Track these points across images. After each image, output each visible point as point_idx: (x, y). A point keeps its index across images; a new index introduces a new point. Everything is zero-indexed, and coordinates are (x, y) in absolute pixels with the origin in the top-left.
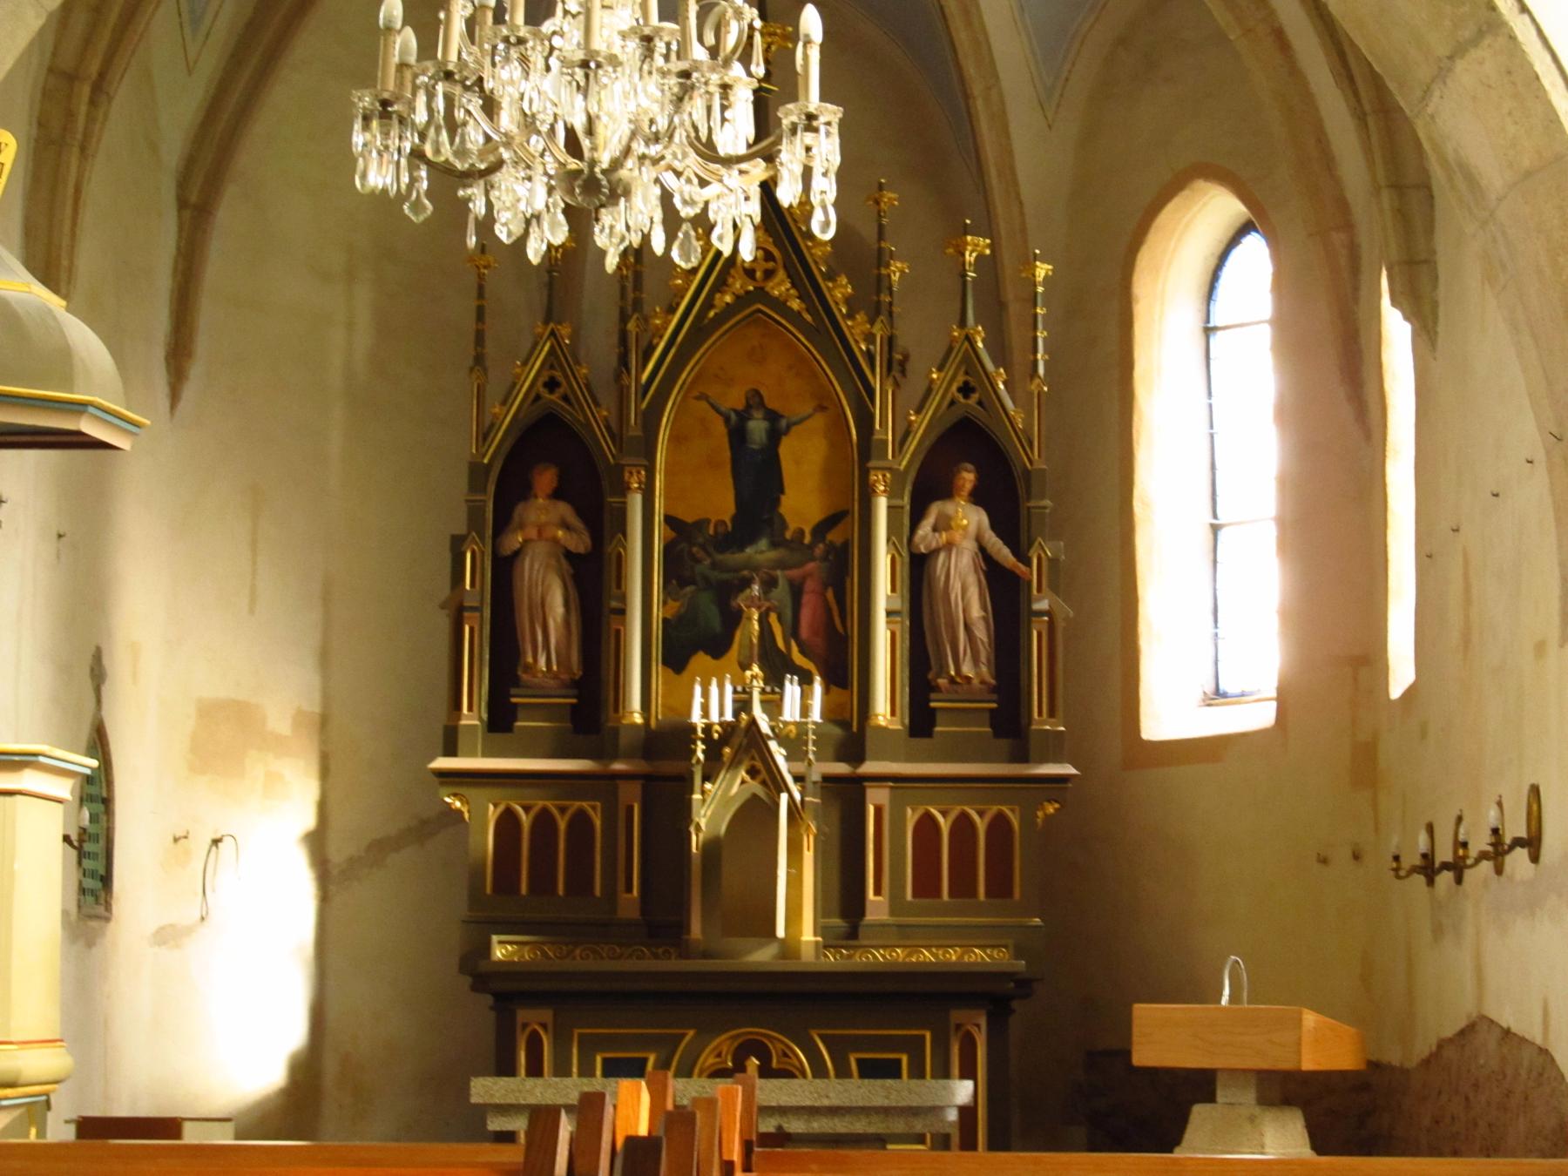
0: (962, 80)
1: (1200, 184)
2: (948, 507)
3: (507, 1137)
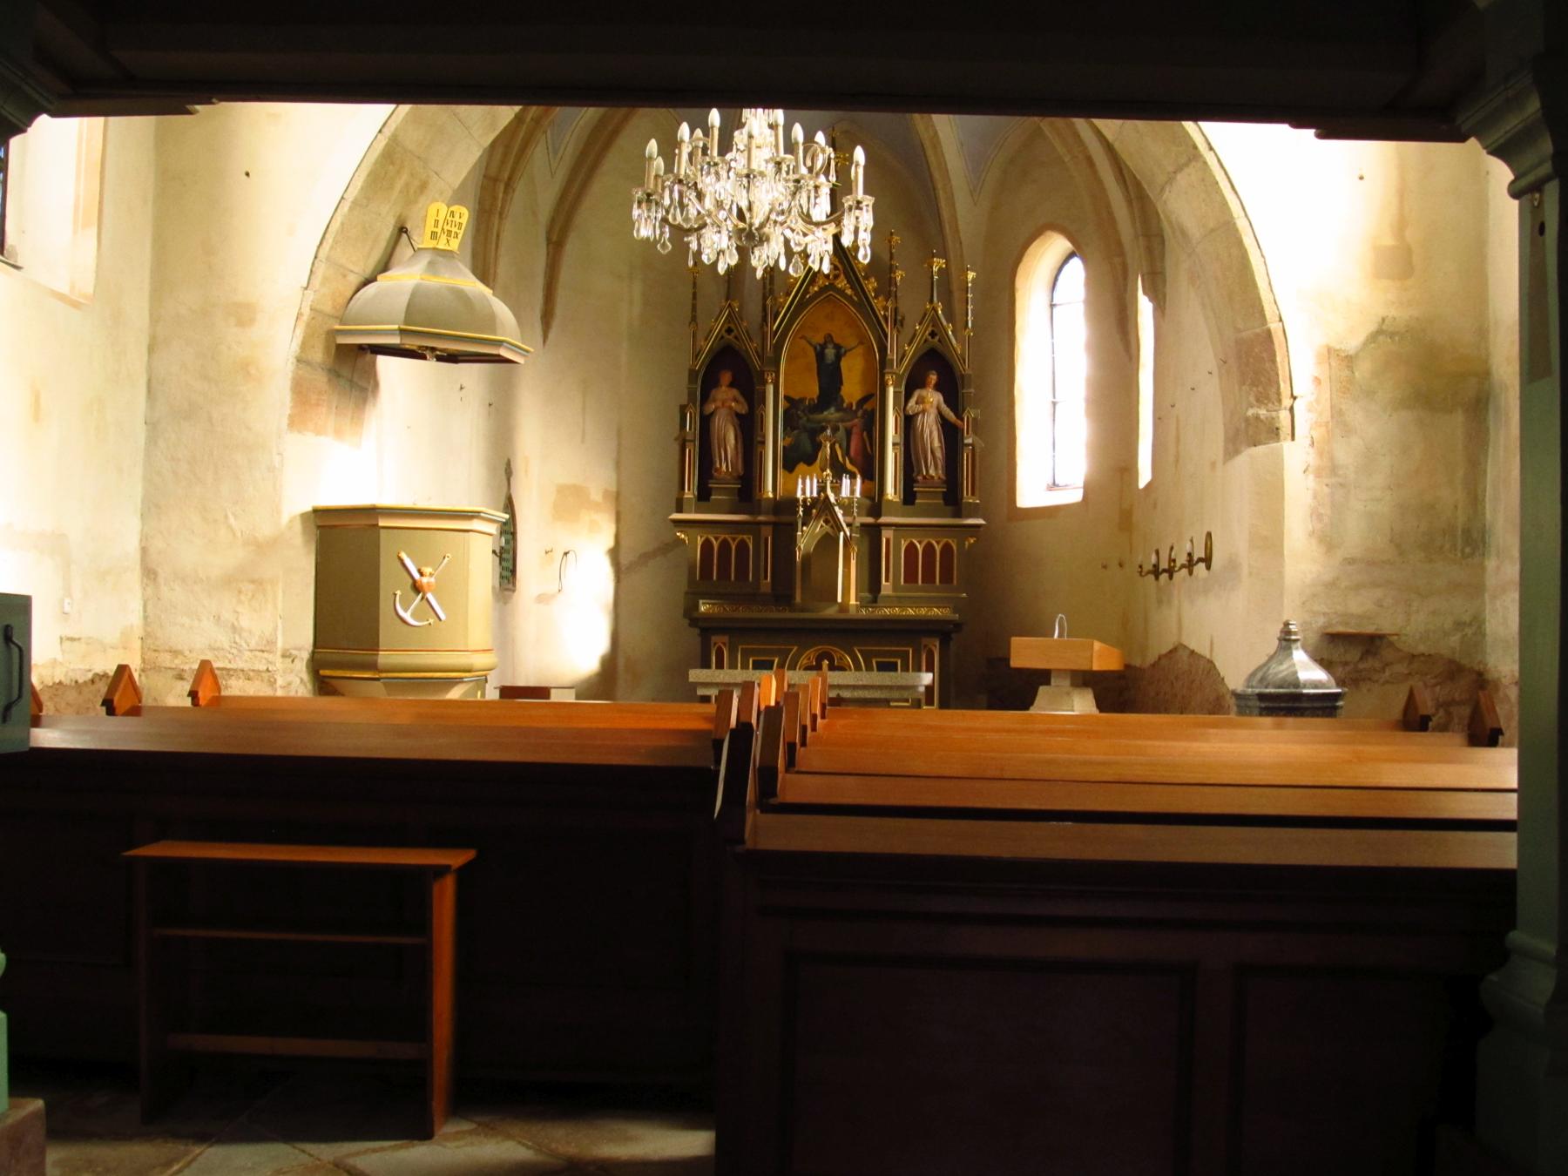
0: (931, 176)
1: (1049, 233)
2: (923, 392)
3: (706, 699)
